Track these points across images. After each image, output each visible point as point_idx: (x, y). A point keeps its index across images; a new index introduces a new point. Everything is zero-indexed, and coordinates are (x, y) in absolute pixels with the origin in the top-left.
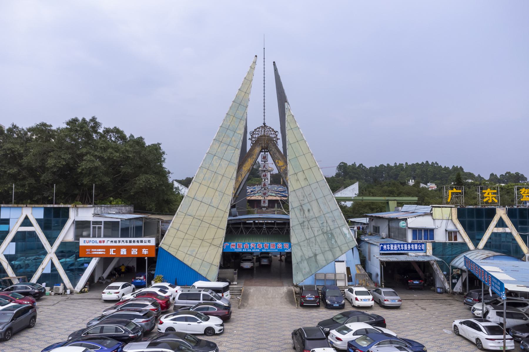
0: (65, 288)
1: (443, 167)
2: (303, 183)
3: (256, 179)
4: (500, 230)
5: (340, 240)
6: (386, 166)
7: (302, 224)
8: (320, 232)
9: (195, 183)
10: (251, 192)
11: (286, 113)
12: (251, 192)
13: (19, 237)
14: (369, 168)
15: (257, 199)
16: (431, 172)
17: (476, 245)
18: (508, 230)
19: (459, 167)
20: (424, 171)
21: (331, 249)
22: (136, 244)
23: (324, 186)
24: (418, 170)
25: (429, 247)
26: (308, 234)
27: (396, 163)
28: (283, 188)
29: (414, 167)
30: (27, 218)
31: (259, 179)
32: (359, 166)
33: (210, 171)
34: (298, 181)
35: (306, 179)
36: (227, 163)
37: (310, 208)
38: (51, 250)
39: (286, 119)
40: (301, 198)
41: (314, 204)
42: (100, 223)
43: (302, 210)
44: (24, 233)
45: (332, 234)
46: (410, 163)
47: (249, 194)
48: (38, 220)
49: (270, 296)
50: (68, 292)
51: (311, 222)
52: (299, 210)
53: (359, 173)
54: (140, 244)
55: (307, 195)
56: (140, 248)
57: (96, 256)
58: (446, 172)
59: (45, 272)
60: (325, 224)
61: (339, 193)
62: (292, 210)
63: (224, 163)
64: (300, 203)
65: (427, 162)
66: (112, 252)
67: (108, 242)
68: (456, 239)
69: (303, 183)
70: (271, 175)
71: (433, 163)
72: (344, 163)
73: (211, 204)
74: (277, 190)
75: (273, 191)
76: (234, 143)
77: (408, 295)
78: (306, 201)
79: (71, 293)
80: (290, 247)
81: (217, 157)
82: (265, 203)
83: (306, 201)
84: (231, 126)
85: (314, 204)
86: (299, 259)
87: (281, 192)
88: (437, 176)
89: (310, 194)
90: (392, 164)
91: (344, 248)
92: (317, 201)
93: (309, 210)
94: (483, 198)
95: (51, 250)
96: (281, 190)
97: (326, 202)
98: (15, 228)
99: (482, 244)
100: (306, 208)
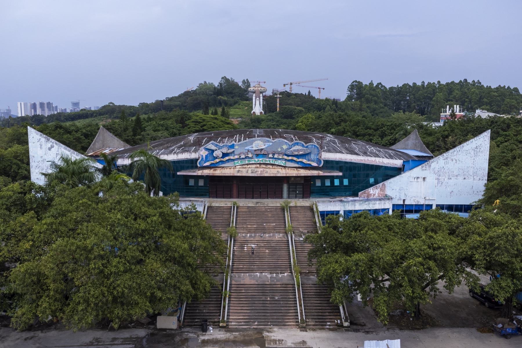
1: (485, 86)
3: (244, 102)
6: (412, 85)
10: (223, 157)
12: (223, 157)
14: (390, 88)
15: (239, 175)
16: (477, 94)
19: (506, 88)
20: (465, 93)
24: (456, 91)
27: (423, 82)
28: (303, 146)
29: (450, 87)
31: (248, 102)
32: (376, 86)
46: (443, 82)
47: (217, 160)
53: (379, 95)
58: (497, 95)
61: (440, 157)
70: (264, 97)
71: (474, 81)
72: (359, 82)
74: (288, 153)
75: (279, 153)
87: (297, 156)
88: (485, 100)
90: (419, 84)
96: (298, 150)
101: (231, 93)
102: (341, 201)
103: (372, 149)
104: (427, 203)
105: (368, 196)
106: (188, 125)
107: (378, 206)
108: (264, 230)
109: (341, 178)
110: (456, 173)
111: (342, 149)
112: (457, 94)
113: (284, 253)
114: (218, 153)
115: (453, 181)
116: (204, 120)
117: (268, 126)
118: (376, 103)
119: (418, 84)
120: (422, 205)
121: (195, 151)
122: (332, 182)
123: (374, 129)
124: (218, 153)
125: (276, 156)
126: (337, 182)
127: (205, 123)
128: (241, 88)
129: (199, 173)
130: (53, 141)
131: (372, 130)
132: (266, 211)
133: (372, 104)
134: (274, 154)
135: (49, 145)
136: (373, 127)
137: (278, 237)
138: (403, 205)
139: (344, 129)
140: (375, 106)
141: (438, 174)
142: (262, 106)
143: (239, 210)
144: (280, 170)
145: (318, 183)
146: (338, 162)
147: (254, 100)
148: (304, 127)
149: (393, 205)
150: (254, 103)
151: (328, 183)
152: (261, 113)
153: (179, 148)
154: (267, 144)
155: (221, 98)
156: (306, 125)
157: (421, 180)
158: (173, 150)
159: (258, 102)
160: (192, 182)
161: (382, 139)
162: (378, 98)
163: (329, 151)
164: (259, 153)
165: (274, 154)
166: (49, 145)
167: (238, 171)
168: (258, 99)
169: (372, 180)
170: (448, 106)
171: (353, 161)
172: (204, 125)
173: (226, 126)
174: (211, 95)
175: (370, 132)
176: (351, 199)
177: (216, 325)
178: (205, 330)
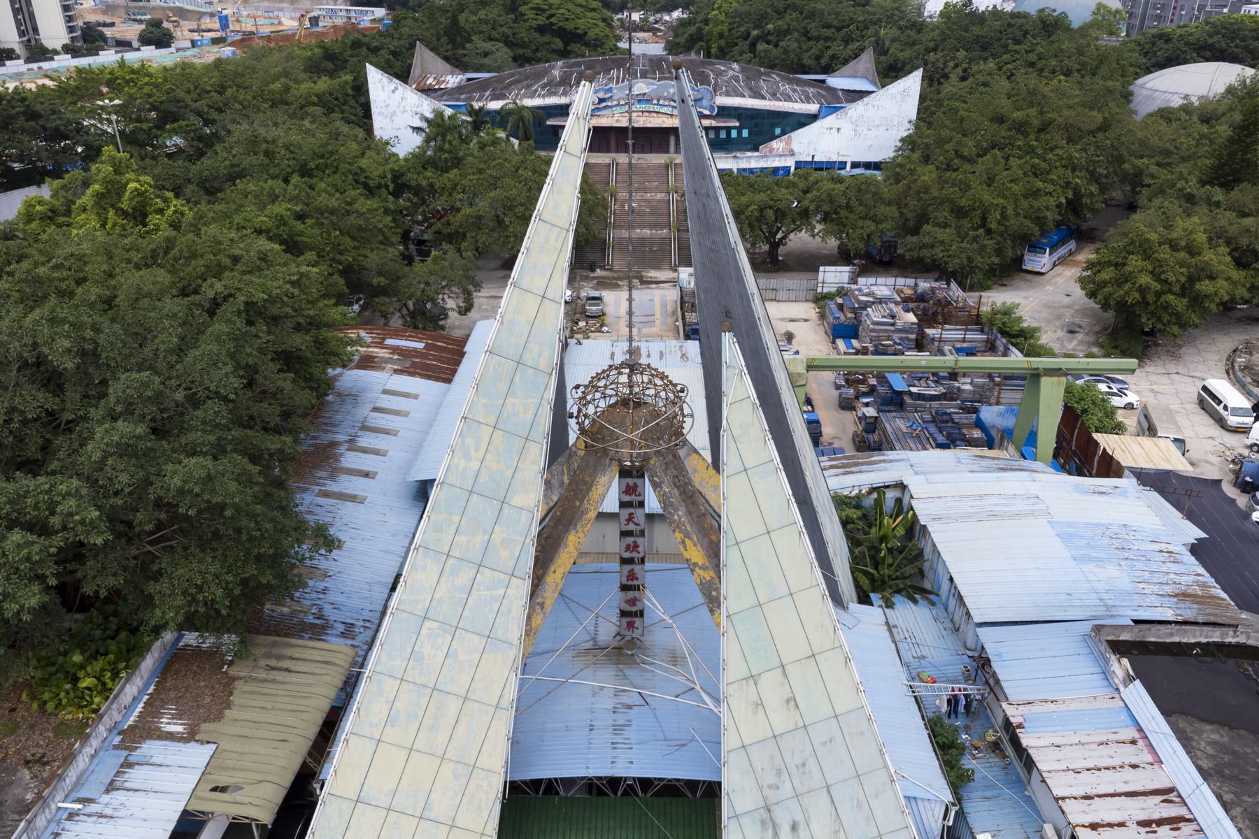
2: (781, 720)
9: (354, 740)
10: (599, 103)
11: (724, 388)
12: (599, 103)
23: (862, 733)
33: (411, 686)
34: (760, 707)
36: (479, 642)
37: (799, 818)
39: (724, 423)
40: (770, 779)
52: (759, 823)
55: (791, 765)
62: (731, 820)
64: (765, 799)
69: (781, 720)
73: (427, 814)
75: (665, 99)
76: (504, 554)
78: (787, 789)
81: (435, 625)
82: (633, 627)
83: (787, 789)
84: (483, 478)
89: (804, 765)
92: (829, 792)
93: (794, 827)
97: (862, 797)
102: (735, 157)
103: (786, 88)
104: (841, 159)
105: (770, 152)
106: (525, 15)
109: (739, 130)
110: (877, 123)
111: (745, 89)
113: (665, 212)
120: (835, 162)
121: (565, 94)
122: (729, 134)
123: (835, 27)
125: (661, 102)
126: (734, 134)
127: (552, 11)
130: (397, 81)
131: (833, 30)
132: (648, 168)
134: (658, 100)
135: (392, 86)
136: (835, 23)
137: (660, 196)
138: (812, 162)
139: (789, 25)
141: (856, 124)
143: (619, 167)
144: (665, 119)
146: (736, 109)
148: (722, 18)
149: (796, 162)
151: (723, 135)
153: (543, 87)
154: (652, 87)
156: (726, 15)
157: (835, 131)
158: (536, 90)
161: (846, 47)
163: (728, 94)
165: (658, 100)
166: (392, 86)
167: (617, 121)
169: (778, 131)
171: (755, 107)
172: (552, 16)
173: (590, 15)
175: (828, 32)
176: (749, 154)
177: (602, 268)
178: (593, 270)
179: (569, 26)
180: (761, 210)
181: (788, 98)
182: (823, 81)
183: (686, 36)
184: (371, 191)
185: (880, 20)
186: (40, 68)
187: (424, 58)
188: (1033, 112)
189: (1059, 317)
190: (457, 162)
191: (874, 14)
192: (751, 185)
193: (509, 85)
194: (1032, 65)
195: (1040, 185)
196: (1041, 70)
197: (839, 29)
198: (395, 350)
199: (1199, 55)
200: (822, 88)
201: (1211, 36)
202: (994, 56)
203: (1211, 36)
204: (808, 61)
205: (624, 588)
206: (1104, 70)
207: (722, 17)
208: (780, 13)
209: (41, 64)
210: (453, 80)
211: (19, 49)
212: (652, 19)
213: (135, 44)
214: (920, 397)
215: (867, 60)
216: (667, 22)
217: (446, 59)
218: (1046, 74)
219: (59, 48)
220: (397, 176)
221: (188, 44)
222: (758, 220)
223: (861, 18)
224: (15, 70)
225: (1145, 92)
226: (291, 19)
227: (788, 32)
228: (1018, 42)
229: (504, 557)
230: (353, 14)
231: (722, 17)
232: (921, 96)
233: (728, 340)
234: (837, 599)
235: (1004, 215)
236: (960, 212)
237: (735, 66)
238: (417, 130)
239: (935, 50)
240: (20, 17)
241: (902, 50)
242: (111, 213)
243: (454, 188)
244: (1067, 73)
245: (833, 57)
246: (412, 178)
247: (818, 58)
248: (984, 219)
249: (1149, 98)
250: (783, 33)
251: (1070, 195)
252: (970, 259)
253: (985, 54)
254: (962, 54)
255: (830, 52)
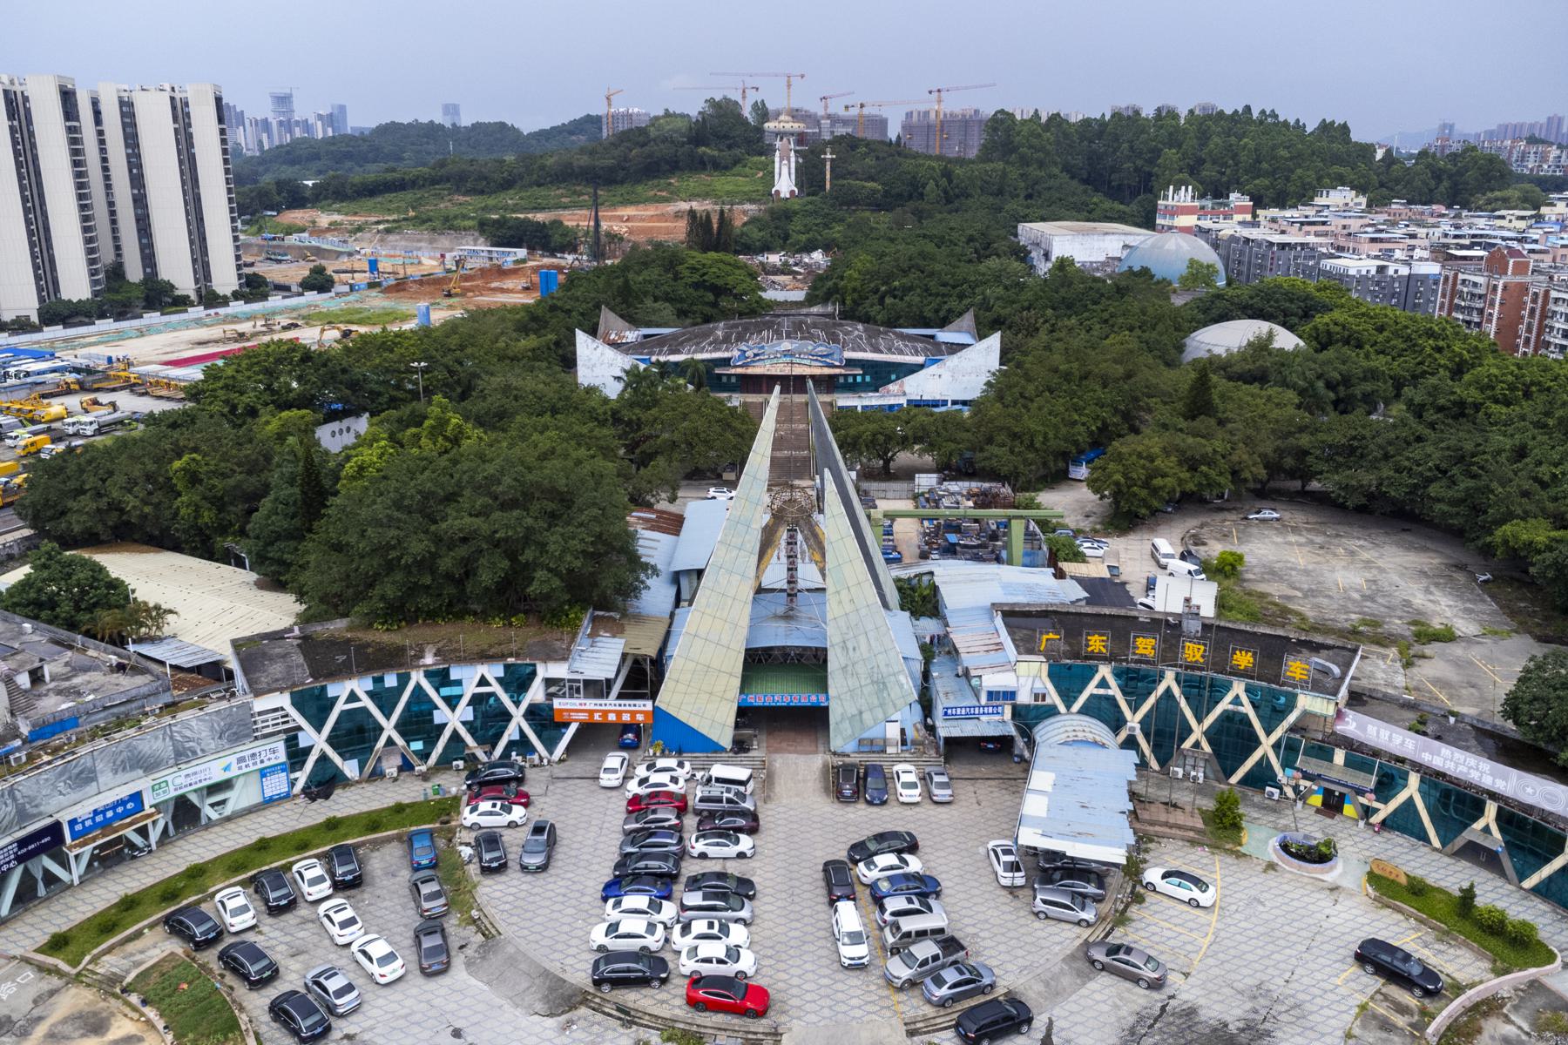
0: (541, 759)
2: (848, 608)
3: (756, 159)
4: (1101, 691)
5: (895, 692)
7: (844, 669)
8: (869, 681)
13: (477, 700)
16: (1249, 150)
17: (1068, 707)
18: (1110, 692)
21: (881, 705)
22: (628, 708)
24: (1216, 139)
25: (1008, 711)
26: (852, 682)
30: (483, 677)
35: (852, 601)
38: (518, 714)
41: (862, 639)
42: (578, 681)
43: (845, 648)
44: (481, 695)
45: (884, 683)
48: (498, 679)
49: (800, 777)
50: (545, 761)
51: (856, 666)
54: (633, 708)
56: (633, 713)
57: (576, 721)
59: (513, 738)
60: (875, 670)
63: (736, 578)
65: (1248, 109)
66: (597, 717)
67: (591, 704)
68: (1044, 699)
69: (848, 608)
71: (1263, 112)
77: (975, 768)
79: (549, 761)
80: (827, 699)
85: (862, 639)
86: (839, 719)
87: (821, 356)
88: (1265, 165)
91: (899, 702)
94: (1087, 646)
95: (518, 714)
98: (470, 689)
99: (1076, 707)
100: (850, 645)
101: (726, 137)
107: (892, 401)
108: (791, 421)
109: (863, 376)
112: (1217, 145)
114: (750, 354)
115: (967, 378)
116: (704, 265)
117: (805, 226)
118: (1041, 165)
119: (1144, 115)
121: (727, 350)
122: (855, 379)
124: (750, 354)
126: (859, 379)
128: (749, 123)
129: (733, 371)
133: (1031, 169)
136: (951, 282)
137: (802, 426)
140: (1038, 173)
142: (793, 177)
145: (842, 380)
147: (777, 165)
150: (777, 170)
151: (850, 380)
152: (792, 192)
153: (710, 344)
155: (704, 153)
159: (785, 170)
160: (724, 379)
162: (1048, 153)
163: (853, 350)
164: (787, 353)
168: (785, 162)
169: (893, 377)
170: (1171, 187)
172: (704, 274)
173: (737, 272)
174: (683, 143)
179: (720, 282)
180: (874, 435)
181: (901, 352)
182: (932, 337)
183: (825, 289)
184: (602, 423)
185: (989, 281)
186: (216, 314)
187: (608, 318)
188: (1075, 365)
189: (1082, 508)
190: (656, 402)
191: (984, 274)
192: (867, 418)
193: (682, 342)
194: (1106, 321)
195: (1077, 417)
196: (1113, 326)
197: (954, 287)
198: (639, 518)
199: (1243, 312)
200: (929, 343)
201: (1252, 298)
202: (1076, 314)
203: (1252, 298)
204: (928, 314)
205: (789, 569)
206: (1160, 327)
207: (856, 275)
208: (905, 272)
209: (218, 310)
210: (631, 336)
211: (193, 296)
212: (791, 261)
213: (295, 288)
214: (965, 546)
215: (968, 319)
216: (806, 264)
217: (622, 316)
218: (1116, 329)
219: (229, 294)
220: (615, 413)
221: (347, 288)
222: (872, 442)
223: (973, 279)
224: (196, 316)
225: (1195, 344)
226: (430, 258)
227: (911, 289)
228: (1095, 303)
229: (748, 546)
230: (495, 255)
231: (856, 275)
232: (1002, 351)
233: (826, 470)
234: (885, 605)
235: (1046, 438)
236: (1015, 436)
237: (860, 327)
238: (618, 379)
239: (1028, 309)
240: (31, 216)
241: (1004, 308)
242: (440, 439)
243: (655, 419)
244: (1131, 329)
245: (950, 311)
246: (627, 415)
247: (937, 311)
248: (1032, 441)
249: (1197, 348)
250: (907, 289)
251: (1099, 424)
252: (1016, 468)
253: (1069, 312)
254: (1049, 312)
255: (946, 307)
